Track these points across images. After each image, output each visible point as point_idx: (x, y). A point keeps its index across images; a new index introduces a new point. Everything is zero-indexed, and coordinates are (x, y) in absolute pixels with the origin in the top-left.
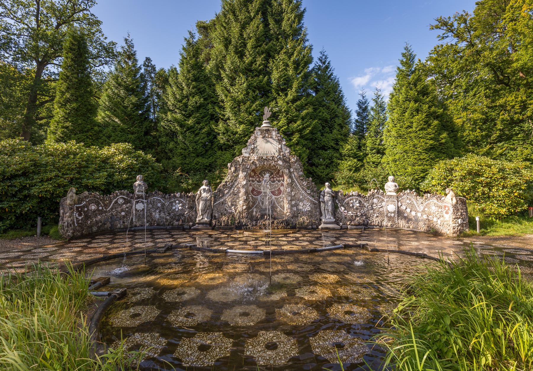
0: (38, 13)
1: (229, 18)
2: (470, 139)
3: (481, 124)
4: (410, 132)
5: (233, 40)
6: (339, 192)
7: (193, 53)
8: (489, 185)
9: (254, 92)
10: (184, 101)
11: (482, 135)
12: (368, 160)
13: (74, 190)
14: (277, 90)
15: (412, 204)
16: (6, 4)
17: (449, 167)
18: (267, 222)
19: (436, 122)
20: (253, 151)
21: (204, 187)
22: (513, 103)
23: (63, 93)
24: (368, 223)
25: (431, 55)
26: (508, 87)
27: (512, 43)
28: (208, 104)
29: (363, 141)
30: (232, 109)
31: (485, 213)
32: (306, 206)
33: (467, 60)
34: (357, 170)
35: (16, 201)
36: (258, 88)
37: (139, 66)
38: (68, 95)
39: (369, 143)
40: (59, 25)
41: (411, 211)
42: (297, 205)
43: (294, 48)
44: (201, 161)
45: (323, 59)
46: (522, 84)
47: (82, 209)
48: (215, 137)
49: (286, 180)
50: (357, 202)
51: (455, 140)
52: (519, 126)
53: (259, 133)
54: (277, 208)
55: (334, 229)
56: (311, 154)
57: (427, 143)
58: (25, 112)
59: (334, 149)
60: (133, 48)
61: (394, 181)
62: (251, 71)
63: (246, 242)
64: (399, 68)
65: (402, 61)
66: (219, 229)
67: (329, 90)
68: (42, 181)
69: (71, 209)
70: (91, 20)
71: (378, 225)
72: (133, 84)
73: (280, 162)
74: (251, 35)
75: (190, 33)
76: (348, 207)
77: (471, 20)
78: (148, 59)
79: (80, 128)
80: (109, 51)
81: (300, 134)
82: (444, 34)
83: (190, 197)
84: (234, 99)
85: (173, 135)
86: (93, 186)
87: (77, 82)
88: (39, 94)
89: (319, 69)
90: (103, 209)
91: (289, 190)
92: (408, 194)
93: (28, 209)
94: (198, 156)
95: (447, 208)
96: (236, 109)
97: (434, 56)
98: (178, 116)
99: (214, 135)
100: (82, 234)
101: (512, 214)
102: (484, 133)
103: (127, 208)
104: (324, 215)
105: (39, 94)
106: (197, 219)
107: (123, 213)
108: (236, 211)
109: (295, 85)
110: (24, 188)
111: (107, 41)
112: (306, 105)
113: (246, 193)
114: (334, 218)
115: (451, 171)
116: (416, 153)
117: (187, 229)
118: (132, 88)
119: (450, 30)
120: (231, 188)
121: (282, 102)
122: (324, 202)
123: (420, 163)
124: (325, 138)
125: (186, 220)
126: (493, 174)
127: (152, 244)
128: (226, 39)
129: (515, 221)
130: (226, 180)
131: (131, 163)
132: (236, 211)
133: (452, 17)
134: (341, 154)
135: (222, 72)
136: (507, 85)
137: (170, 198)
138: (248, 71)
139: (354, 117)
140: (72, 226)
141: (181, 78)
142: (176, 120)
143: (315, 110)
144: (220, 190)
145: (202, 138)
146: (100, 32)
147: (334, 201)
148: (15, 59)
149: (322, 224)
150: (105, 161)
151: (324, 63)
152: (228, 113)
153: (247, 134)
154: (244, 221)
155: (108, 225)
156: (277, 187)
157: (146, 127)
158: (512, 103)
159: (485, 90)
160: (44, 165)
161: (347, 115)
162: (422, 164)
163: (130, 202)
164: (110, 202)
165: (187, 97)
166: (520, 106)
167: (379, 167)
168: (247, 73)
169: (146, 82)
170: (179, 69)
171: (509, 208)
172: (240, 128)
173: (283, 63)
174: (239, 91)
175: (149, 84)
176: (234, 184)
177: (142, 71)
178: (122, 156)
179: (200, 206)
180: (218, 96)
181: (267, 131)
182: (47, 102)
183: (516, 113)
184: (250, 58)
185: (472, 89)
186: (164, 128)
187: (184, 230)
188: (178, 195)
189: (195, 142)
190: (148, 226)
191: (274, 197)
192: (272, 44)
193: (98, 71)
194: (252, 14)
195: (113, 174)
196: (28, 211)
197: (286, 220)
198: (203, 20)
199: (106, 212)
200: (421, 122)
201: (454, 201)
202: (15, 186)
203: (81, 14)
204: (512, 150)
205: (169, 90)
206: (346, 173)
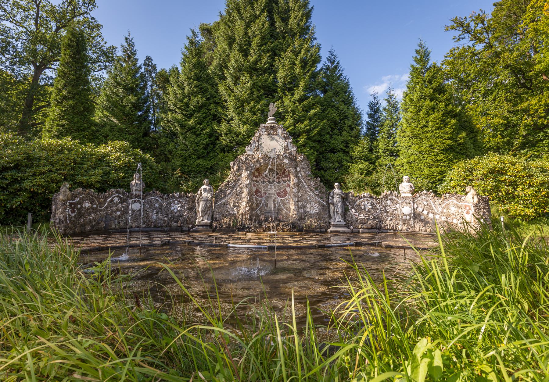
0: (37, 16)
1: (233, 16)
2: (490, 146)
3: (502, 129)
4: (425, 131)
5: (237, 38)
6: (349, 193)
7: (196, 57)
8: (513, 184)
9: (259, 91)
10: (185, 101)
11: (503, 142)
12: (381, 163)
13: (68, 185)
14: (283, 89)
15: (429, 207)
16: (6, 7)
17: (469, 166)
18: (272, 224)
19: (453, 121)
20: (257, 148)
21: (204, 186)
22: (537, 107)
23: (60, 91)
24: (381, 226)
25: (447, 59)
26: (530, 91)
27: (533, 45)
28: (210, 104)
29: (375, 143)
30: (236, 108)
31: (510, 214)
32: (313, 208)
33: (485, 62)
34: (369, 173)
35: (7, 195)
36: (263, 87)
37: (139, 65)
38: (64, 93)
39: (381, 145)
40: (58, 28)
41: (428, 213)
42: (304, 207)
43: (301, 46)
44: (201, 163)
45: (332, 59)
46: (546, 87)
47: (75, 206)
48: (217, 139)
49: (293, 179)
50: (369, 204)
51: (474, 141)
52: (544, 132)
53: (264, 130)
54: (282, 210)
55: (344, 233)
56: (319, 157)
57: (445, 143)
58: (20, 117)
59: (344, 151)
60: (134, 47)
61: (409, 181)
62: (256, 70)
63: (249, 241)
64: (412, 66)
65: (416, 58)
66: (220, 231)
67: (338, 90)
68: (34, 175)
69: (63, 205)
70: (91, 24)
71: (392, 229)
72: (133, 83)
73: (286, 161)
74: (256, 33)
75: (193, 32)
76: (359, 209)
77: (489, 20)
78: (148, 58)
79: (76, 127)
80: (108, 55)
81: (308, 135)
82: (460, 35)
83: (189, 197)
84: (237, 99)
85: (173, 135)
86: (88, 184)
87: (75, 80)
88: (36, 99)
89: (327, 69)
90: (97, 207)
91: (295, 190)
92: (424, 195)
93: (18, 203)
94: (199, 158)
95: (468, 208)
96: (240, 109)
97: (450, 59)
98: (179, 116)
99: (216, 136)
100: (74, 232)
101: (540, 216)
102: (505, 140)
103: (123, 207)
104: (333, 218)
105: (36, 99)
106: (197, 221)
107: (118, 213)
108: (238, 213)
109: (302, 84)
110: (16, 181)
111: (107, 45)
112: (314, 105)
113: (250, 193)
114: (345, 221)
115: (471, 171)
116: (432, 154)
117: (186, 231)
118: (131, 87)
119: (467, 30)
120: (233, 188)
121: (288, 101)
122: (333, 204)
123: (437, 164)
124: (333, 139)
125: (185, 222)
126: (518, 172)
127: (148, 241)
128: (230, 38)
129: (543, 223)
130: (228, 179)
131: (128, 160)
132: (238, 213)
133: (468, 16)
134: (351, 157)
135: (225, 71)
136: (529, 89)
137: (168, 198)
138: (253, 70)
139: (365, 118)
140: (64, 223)
141: (182, 77)
142: (176, 120)
143: (323, 111)
144: (221, 191)
145: (204, 139)
146: (100, 37)
147: (344, 203)
148: (13, 63)
149: (332, 227)
150: (101, 158)
151: (333, 63)
152: (231, 113)
153: (250, 134)
154: (247, 223)
155: (102, 225)
156: (282, 188)
157: (145, 128)
158: (535, 106)
159: (506, 93)
160: (37, 159)
161: (357, 117)
162: (439, 165)
163: (126, 201)
164: (105, 201)
165: (188, 96)
166: (543, 110)
167: (393, 170)
168: (251, 72)
169: (146, 82)
170: (180, 69)
171: (537, 209)
172: (244, 129)
173: (290, 61)
174: (243, 90)
175: (150, 83)
176: (236, 184)
177: (142, 70)
178: (119, 154)
179: (200, 207)
180: (220, 96)
181: (273, 127)
182: (43, 107)
183: (540, 118)
184: (255, 57)
185: (492, 93)
186: (164, 128)
187: (182, 231)
188: (177, 195)
189: (196, 143)
190: (145, 227)
191: (279, 199)
192: (279, 42)
193: (97, 76)
194: (258, 13)
195: (109, 172)
196: (19, 205)
197: (292, 223)
198: (205, 23)
199: (100, 210)
200: (438, 121)
201: (476, 200)
202: (6, 179)
203: (81, 18)
204: (537, 158)
205: (170, 90)
206: (357, 176)
